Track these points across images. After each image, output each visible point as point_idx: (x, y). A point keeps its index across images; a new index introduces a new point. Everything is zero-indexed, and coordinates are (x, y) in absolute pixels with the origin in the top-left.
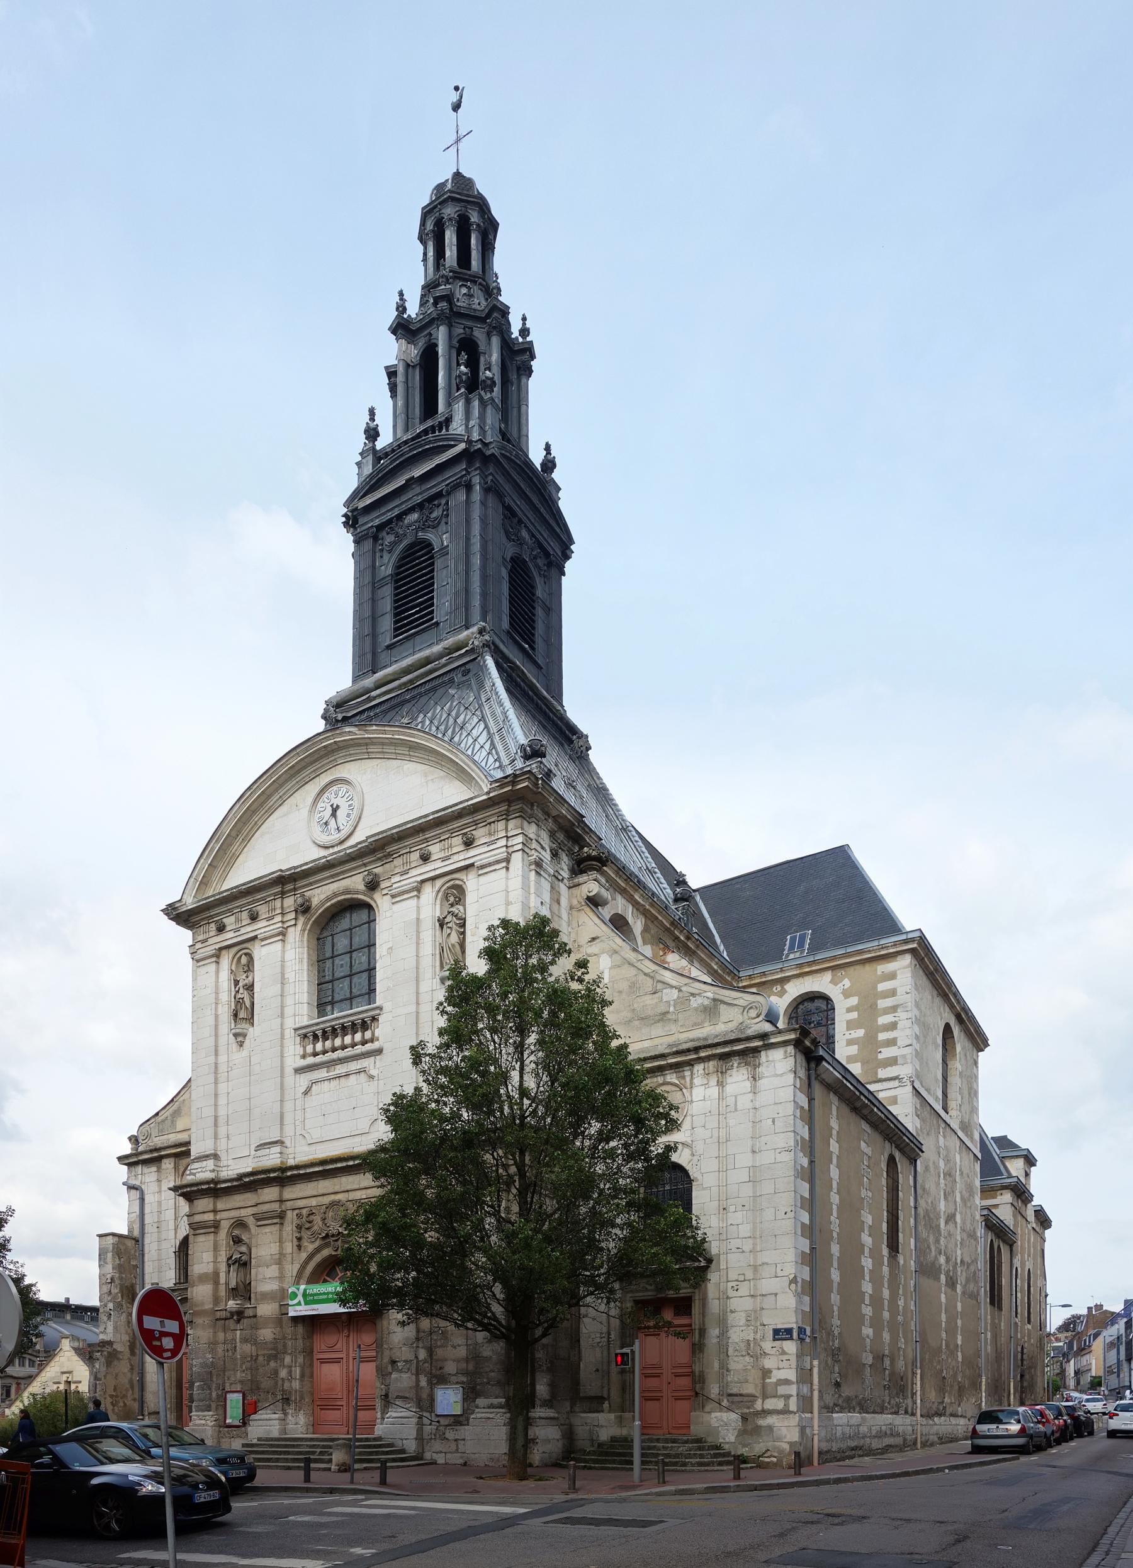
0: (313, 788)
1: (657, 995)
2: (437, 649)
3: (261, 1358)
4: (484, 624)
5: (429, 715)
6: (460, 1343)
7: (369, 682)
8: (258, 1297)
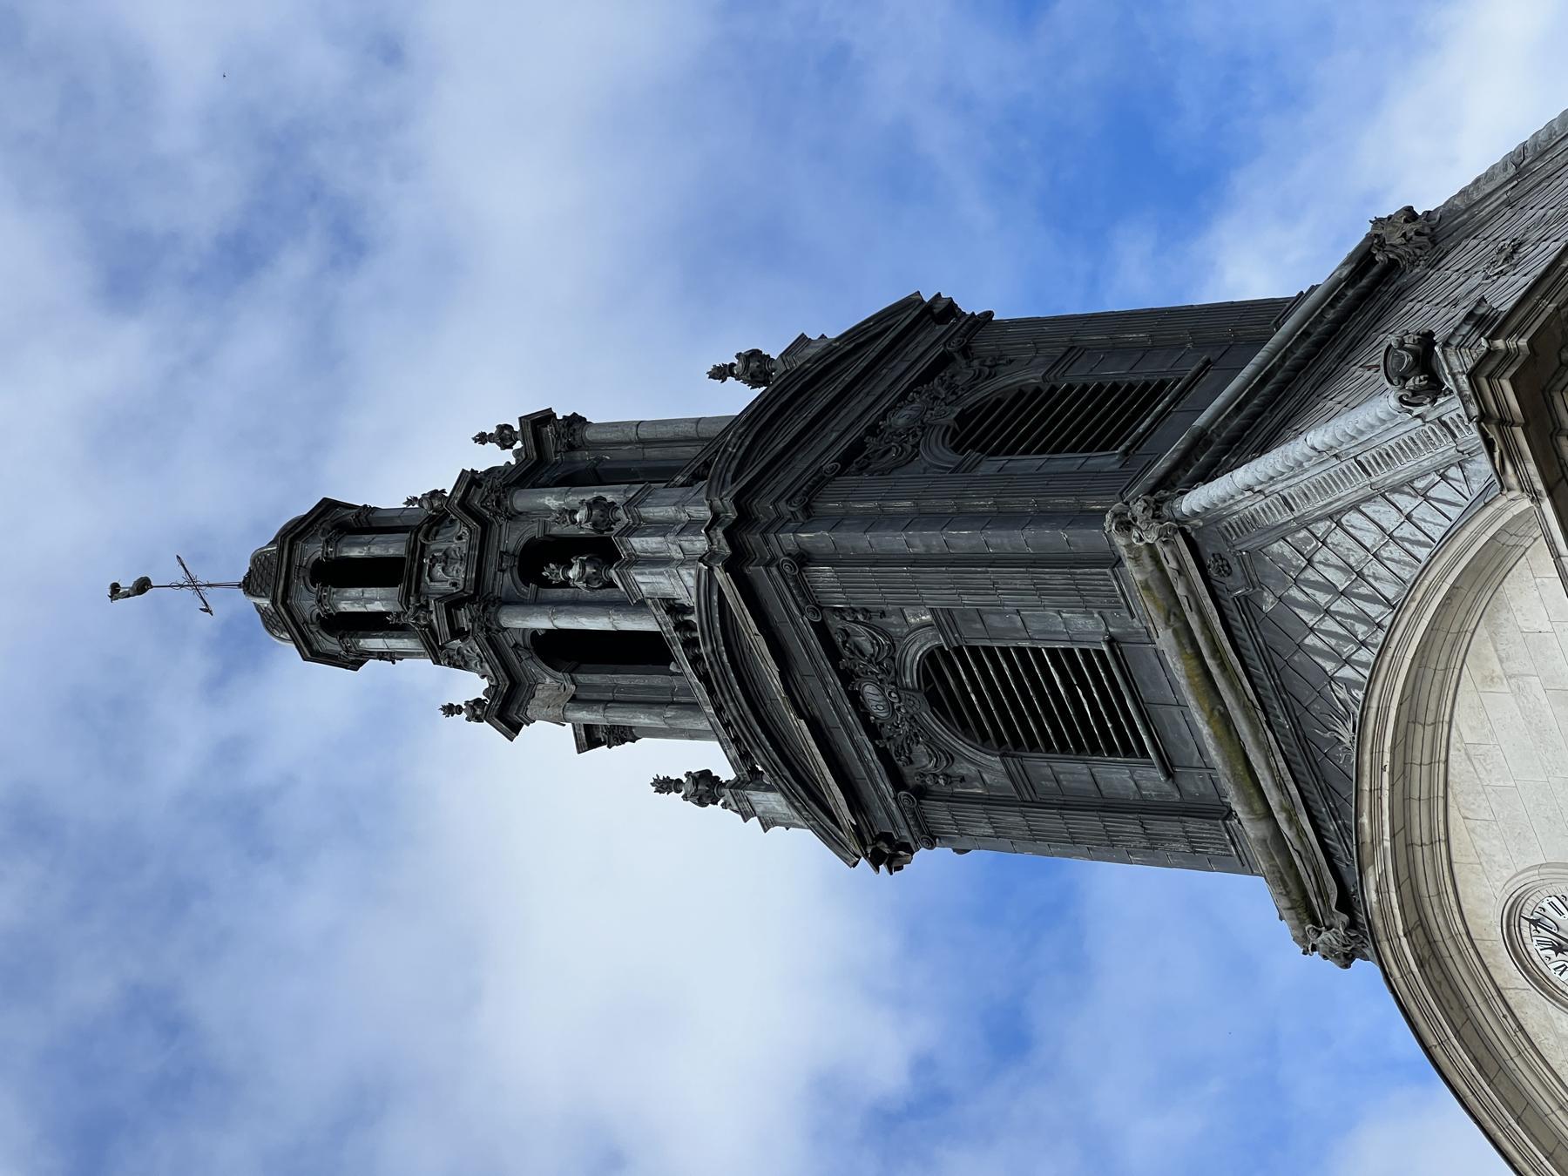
0: (1534, 1010)
4: (1108, 517)
5: (1329, 666)
7: (1252, 830)
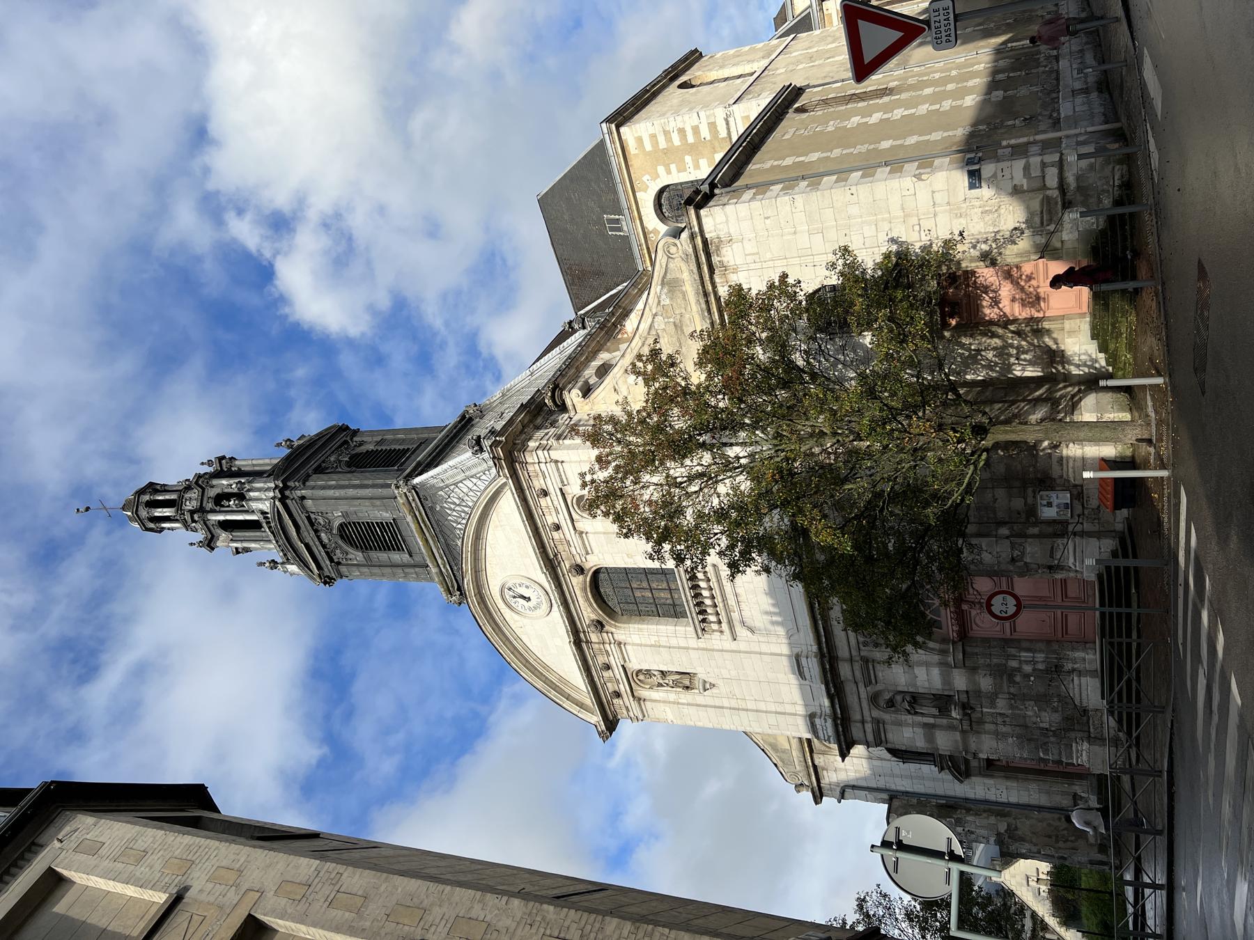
1: (660, 334)
2: (409, 518)
3: (1012, 690)
5: (455, 525)
6: (990, 495)
8: (947, 688)
